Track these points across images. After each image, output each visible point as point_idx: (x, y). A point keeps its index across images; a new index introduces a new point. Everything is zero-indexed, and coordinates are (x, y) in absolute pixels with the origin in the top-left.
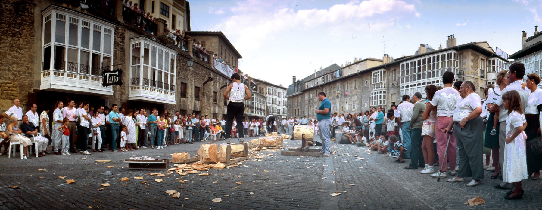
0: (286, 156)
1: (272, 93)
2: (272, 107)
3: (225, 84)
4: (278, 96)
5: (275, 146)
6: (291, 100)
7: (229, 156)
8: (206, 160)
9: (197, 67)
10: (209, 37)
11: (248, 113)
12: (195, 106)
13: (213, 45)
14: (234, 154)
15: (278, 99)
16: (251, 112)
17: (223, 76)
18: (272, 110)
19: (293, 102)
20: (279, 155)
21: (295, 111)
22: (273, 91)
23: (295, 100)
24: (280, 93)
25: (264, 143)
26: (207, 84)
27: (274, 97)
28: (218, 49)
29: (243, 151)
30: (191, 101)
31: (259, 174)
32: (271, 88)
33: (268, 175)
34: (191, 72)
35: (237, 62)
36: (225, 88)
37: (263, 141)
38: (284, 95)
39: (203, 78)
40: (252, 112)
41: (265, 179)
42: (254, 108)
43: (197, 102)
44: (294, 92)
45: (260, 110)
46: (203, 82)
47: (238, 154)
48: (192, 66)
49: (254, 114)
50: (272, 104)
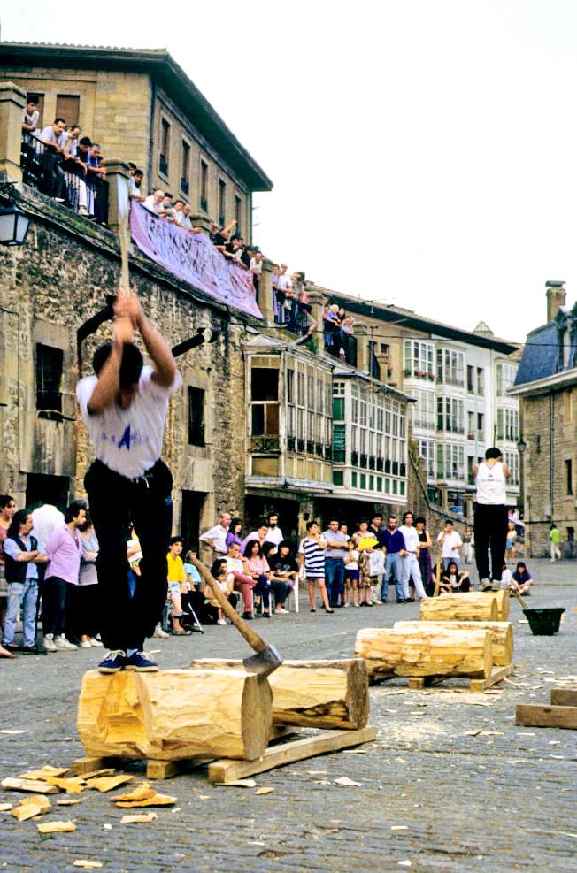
0: (542, 731)
1: (435, 372)
2: (440, 446)
3: (193, 334)
4: (470, 387)
5: (480, 675)
6: (545, 407)
7: (263, 729)
8: (159, 750)
9: (43, 244)
10: (102, 77)
11: (314, 484)
12: (38, 451)
13: (119, 119)
14: (298, 717)
15: (469, 402)
16: (330, 477)
17: (180, 295)
18: (440, 462)
19: (552, 423)
20: (506, 722)
21: (564, 470)
22: (439, 359)
23: (563, 411)
24: (480, 370)
25: (421, 656)
26: (99, 332)
27: (449, 391)
28: (146, 143)
29: (342, 703)
30: (15, 425)
31: (423, 826)
32: (428, 343)
33: (468, 830)
34: (14, 270)
35: (243, 209)
36: (192, 351)
37: (415, 647)
38: (499, 380)
39: (77, 304)
40: (338, 478)
41: (457, 849)
42: (348, 456)
43: (49, 427)
44: (559, 369)
45: (380, 468)
46: (80, 323)
47: (318, 715)
48: (20, 238)
49: (347, 491)
50: (440, 427)
